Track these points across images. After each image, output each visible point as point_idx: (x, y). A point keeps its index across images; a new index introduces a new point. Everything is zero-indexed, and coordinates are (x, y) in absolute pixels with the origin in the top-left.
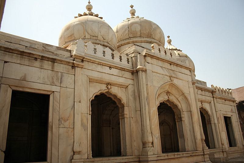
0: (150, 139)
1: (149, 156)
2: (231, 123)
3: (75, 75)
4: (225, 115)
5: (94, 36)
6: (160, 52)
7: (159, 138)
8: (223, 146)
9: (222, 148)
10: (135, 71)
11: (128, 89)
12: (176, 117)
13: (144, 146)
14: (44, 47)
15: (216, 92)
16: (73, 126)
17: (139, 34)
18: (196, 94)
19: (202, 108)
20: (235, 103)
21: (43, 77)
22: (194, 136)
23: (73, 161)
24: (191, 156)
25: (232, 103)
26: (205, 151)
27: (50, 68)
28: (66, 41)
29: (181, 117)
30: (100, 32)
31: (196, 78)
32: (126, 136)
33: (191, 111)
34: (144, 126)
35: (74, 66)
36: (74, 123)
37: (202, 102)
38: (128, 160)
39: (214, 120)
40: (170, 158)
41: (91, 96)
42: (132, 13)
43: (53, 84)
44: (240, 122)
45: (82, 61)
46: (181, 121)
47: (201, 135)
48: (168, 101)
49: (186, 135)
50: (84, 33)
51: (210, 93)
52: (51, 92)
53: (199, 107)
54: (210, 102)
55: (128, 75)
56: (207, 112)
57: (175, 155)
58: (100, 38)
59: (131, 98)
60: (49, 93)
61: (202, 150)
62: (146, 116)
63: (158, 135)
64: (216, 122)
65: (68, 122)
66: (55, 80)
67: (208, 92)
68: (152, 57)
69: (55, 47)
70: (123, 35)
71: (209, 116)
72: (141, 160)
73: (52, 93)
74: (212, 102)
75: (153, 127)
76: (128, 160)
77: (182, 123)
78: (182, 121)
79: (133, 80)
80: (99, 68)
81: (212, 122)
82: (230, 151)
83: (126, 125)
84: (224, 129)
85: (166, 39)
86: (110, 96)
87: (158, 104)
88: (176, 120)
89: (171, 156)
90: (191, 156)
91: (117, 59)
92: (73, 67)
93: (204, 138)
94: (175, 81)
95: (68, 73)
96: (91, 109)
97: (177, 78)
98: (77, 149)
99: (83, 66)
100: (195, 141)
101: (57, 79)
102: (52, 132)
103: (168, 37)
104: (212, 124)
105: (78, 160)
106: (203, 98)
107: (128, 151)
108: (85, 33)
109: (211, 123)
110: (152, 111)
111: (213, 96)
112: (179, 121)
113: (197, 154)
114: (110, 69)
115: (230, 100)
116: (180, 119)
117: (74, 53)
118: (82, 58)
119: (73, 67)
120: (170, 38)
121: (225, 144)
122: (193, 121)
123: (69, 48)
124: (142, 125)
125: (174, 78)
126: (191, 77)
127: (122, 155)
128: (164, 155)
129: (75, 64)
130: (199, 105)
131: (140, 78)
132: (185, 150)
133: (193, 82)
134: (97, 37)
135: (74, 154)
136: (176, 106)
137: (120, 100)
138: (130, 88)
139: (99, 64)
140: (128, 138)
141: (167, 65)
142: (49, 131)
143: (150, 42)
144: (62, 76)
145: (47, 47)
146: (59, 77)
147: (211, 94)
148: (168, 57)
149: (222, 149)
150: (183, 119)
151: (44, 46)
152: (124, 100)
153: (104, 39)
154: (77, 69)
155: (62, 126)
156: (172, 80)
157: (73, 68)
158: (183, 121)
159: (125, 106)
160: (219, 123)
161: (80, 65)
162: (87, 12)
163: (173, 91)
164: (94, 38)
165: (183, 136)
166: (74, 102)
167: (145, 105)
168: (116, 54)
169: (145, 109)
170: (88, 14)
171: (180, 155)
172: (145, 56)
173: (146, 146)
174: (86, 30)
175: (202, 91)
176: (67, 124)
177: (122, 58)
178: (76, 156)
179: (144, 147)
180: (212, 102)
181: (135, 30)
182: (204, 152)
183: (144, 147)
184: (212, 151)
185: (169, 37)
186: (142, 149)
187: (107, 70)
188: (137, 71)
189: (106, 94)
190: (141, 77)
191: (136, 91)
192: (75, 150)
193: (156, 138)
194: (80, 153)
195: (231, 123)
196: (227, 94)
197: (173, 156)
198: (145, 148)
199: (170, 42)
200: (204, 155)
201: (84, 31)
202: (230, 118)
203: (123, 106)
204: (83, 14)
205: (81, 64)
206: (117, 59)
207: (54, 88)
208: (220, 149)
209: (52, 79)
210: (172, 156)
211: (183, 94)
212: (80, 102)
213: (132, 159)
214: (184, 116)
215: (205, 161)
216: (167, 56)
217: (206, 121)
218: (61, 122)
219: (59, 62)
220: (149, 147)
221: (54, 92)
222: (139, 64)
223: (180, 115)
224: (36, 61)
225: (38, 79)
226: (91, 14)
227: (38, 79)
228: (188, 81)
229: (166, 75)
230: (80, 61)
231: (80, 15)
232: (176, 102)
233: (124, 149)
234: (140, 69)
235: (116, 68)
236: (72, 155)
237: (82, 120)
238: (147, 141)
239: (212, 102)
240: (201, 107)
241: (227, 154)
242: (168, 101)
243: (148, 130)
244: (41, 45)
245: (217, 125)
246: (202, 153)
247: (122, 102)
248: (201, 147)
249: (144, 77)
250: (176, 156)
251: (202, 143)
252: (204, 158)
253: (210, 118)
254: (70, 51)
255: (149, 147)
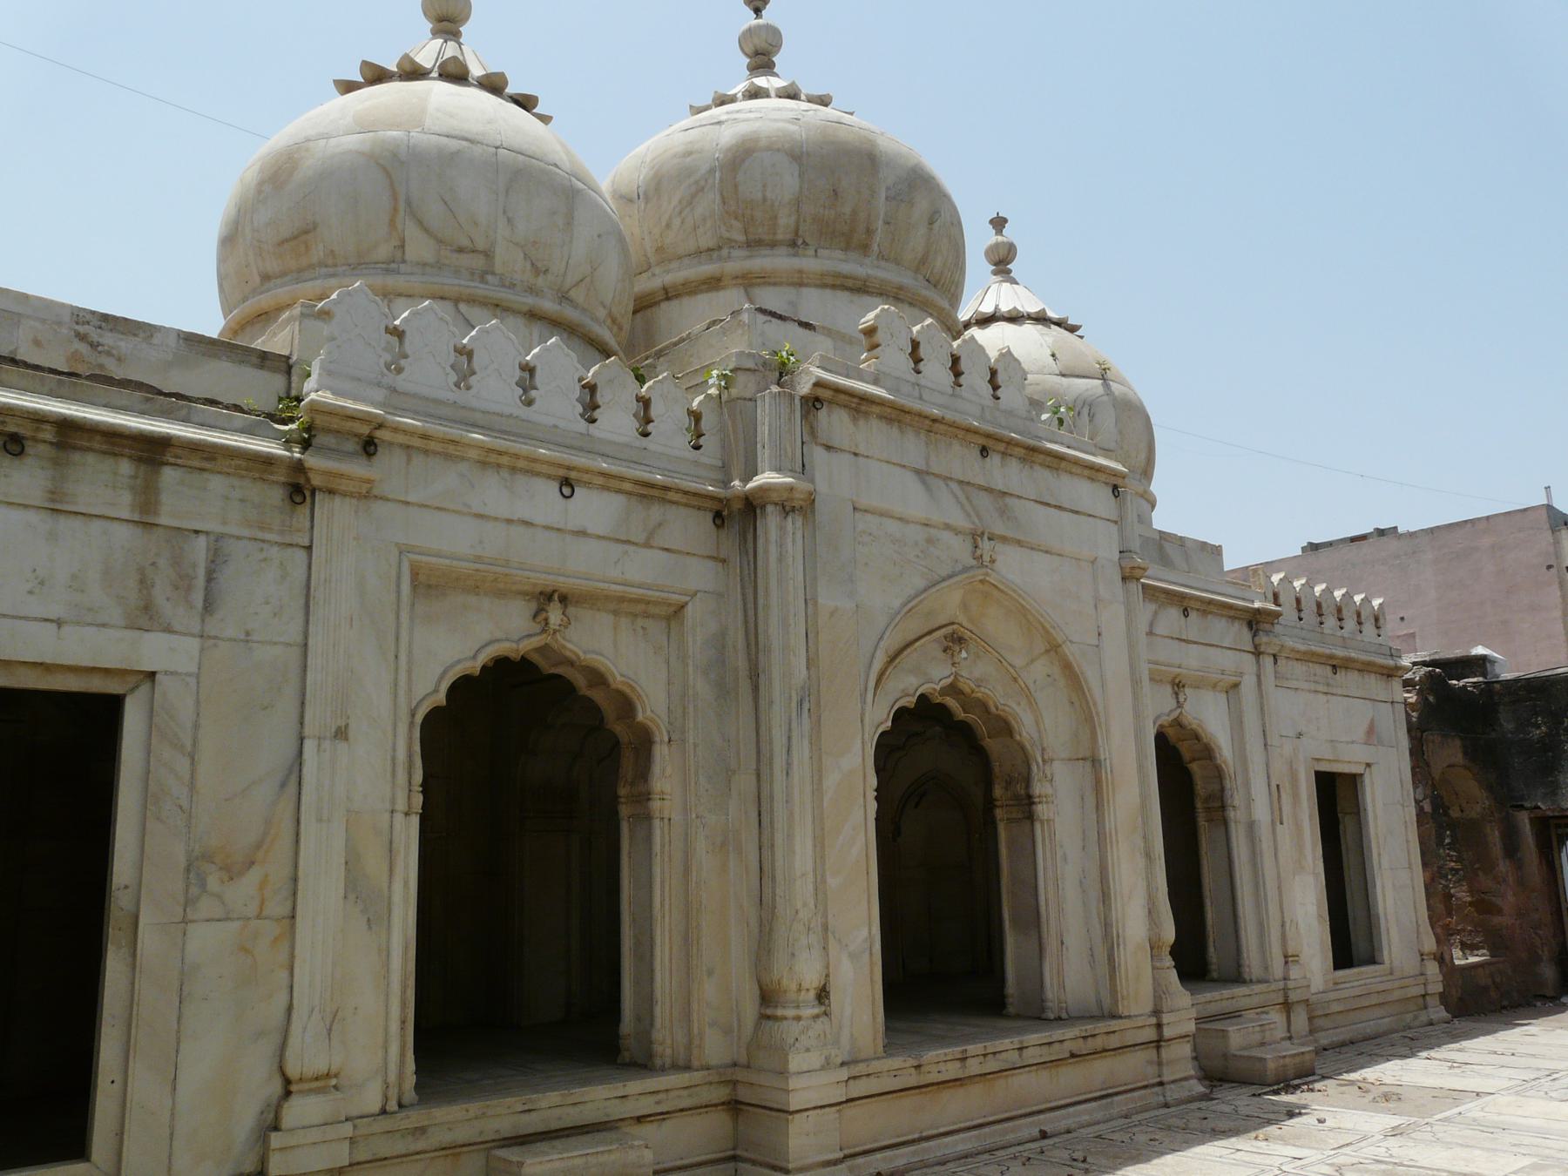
0: (808, 972)
1: (793, 1083)
2: (1357, 811)
3: (309, 548)
4: (1325, 767)
5: (461, 250)
6: (921, 366)
7: (866, 957)
8: (1295, 973)
9: (1286, 979)
10: (737, 506)
11: (682, 624)
12: (998, 791)
13: (769, 1012)
14: (82, 337)
15: (1278, 615)
16: (289, 904)
17: (786, 221)
18: (1143, 638)
19: (1178, 723)
20: (1397, 685)
21: (74, 577)
22: (1107, 925)
23: (276, 1140)
24: (1073, 1055)
25: (1374, 685)
26: (1166, 1019)
27: (123, 504)
28: (272, 266)
29: (1029, 797)
30: (509, 220)
31: (1162, 520)
32: (652, 939)
33: (1095, 762)
34: (774, 878)
35: (302, 481)
36: (295, 880)
37: (1178, 686)
38: (658, 1103)
39: (1249, 801)
40: (934, 1078)
41: (430, 689)
42: (757, 53)
43: (145, 616)
44: (1417, 802)
45: (369, 447)
46: (1030, 817)
47: (1151, 912)
48: (953, 689)
49: (1053, 915)
50: (392, 223)
51: (1237, 624)
52: (132, 679)
53: (1158, 717)
54: (1236, 686)
55: (689, 528)
56: (1207, 752)
57: (969, 1062)
58: (508, 260)
59: (702, 687)
60: (112, 687)
61: (1149, 1008)
62: (791, 814)
63: (864, 933)
64: (1261, 812)
65: (253, 876)
66: (161, 593)
67: (1224, 621)
68: (860, 405)
69: (172, 341)
70: (677, 222)
71: (1219, 774)
72: (744, 1094)
73: (137, 687)
74: (1249, 682)
75: (833, 882)
76: (658, 1103)
77: (1033, 831)
78: (1038, 826)
79: (724, 561)
80: (493, 494)
81: (1236, 816)
82: (1332, 996)
83: (657, 870)
84: (1310, 858)
85: (977, 240)
86: (559, 670)
87: (879, 717)
88: (999, 813)
89: (942, 1067)
90: (1073, 1055)
91: (616, 422)
92: (299, 490)
93: (1169, 933)
94: (1011, 565)
95: (260, 535)
96: (418, 777)
97: (1019, 543)
98: (307, 1057)
99: (369, 481)
100: (1111, 958)
101: (183, 584)
102: (134, 955)
103: (991, 222)
104: (1232, 826)
105: (315, 1135)
106: (1190, 660)
107: (666, 1037)
108: (400, 227)
109: (1225, 823)
110: (831, 780)
111: (1256, 647)
112: (1020, 816)
113: (1114, 1041)
114: (566, 491)
115: (1366, 668)
116: (1026, 805)
117: (315, 392)
118: (365, 430)
119: (299, 490)
120: (1009, 233)
121: (1303, 958)
122: (1109, 825)
123: (276, 340)
124: (764, 872)
125: (1000, 547)
126: (1121, 531)
127: (626, 1056)
128: (896, 1062)
129: (311, 475)
130: (1159, 706)
131: (766, 551)
132: (1043, 1010)
133: (1127, 564)
134: (488, 254)
135: (288, 1094)
136: (1004, 728)
137: (626, 705)
138: (700, 621)
139: (489, 461)
140: (664, 954)
141: (959, 460)
142: (109, 945)
143: (859, 284)
144: (216, 559)
145: (108, 339)
146: (194, 566)
147: (1238, 634)
148: (972, 405)
149: (1285, 990)
150: (1041, 810)
151: (81, 329)
152: (653, 705)
153: (537, 271)
154: (333, 517)
155: (206, 907)
156: (986, 558)
157: (298, 499)
158: (1042, 822)
159: (657, 739)
160: (1277, 819)
161: (350, 478)
162: (429, 52)
163: (997, 626)
164: (465, 260)
165: (1032, 921)
166: (302, 739)
167: (789, 738)
168: (611, 381)
169: (789, 764)
170: (428, 65)
171: (1004, 1055)
172: (813, 403)
173: (779, 1012)
174: (409, 203)
175: (1186, 613)
176: (243, 891)
177: (654, 412)
178: (301, 1110)
179: (768, 1017)
180: (1242, 686)
181: (765, 199)
182: (1159, 1026)
183: (768, 1017)
184: (1218, 998)
185: (999, 223)
186: (757, 1026)
187: (542, 500)
188: (752, 507)
189: (536, 658)
190: (773, 549)
191: (737, 637)
192: (293, 1071)
193: (853, 956)
194: (334, 1082)
195: (1358, 813)
196: (1350, 624)
197: (958, 1064)
198: (770, 1023)
199: (1002, 261)
200: (1158, 1043)
201: (395, 210)
202: (1353, 780)
203: (644, 742)
204: (392, 67)
205: (357, 468)
206: (616, 422)
207: (151, 651)
208: (1273, 987)
209: (142, 581)
210: (950, 1066)
211: (1054, 648)
212: (341, 734)
213: (685, 1093)
214: (1049, 791)
215: (1161, 1084)
216: (963, 391)
217: (1199, 805)
218: (203, 885)
219: (196, 463)
220: (798, 1018)
221: (152, 675)
222: (764, 455)
223: (1028, 781)
224: (17, 462)
225: (30, 592)
226: (455, 74)
227: (30, 592)
228: (1093, 562)
229: (947, 527)
230: (351, 446)
231: (377, 76)
232: (1000, 696)
233: (638, 1019)
234: (775, 497)
235: (609, 483)
236: (274, 1100)
237: (352, 863)
238: (785, 982)
239: (1249, 682)
240: (1165, 720)
241: (1311, 1019)
242: (953, 689)
243: (799, 905)
244: (60, 324)
245: (1264, 832)
246: (1150, 1034)
247: (640, 717)
248: (1146, 988)
249: (794, 549)
250: (974, 1067)
251: (1154, 968)
252: (1160, 1064)
253: (1222, 790)
254: (285, 365)
255: (798, 1018)
